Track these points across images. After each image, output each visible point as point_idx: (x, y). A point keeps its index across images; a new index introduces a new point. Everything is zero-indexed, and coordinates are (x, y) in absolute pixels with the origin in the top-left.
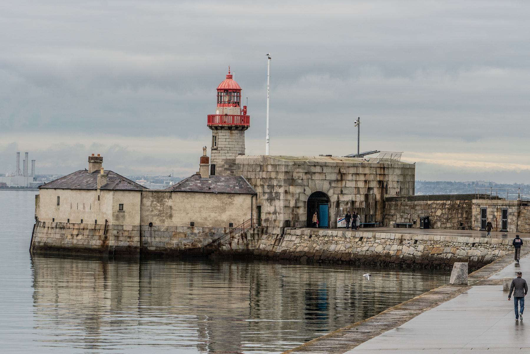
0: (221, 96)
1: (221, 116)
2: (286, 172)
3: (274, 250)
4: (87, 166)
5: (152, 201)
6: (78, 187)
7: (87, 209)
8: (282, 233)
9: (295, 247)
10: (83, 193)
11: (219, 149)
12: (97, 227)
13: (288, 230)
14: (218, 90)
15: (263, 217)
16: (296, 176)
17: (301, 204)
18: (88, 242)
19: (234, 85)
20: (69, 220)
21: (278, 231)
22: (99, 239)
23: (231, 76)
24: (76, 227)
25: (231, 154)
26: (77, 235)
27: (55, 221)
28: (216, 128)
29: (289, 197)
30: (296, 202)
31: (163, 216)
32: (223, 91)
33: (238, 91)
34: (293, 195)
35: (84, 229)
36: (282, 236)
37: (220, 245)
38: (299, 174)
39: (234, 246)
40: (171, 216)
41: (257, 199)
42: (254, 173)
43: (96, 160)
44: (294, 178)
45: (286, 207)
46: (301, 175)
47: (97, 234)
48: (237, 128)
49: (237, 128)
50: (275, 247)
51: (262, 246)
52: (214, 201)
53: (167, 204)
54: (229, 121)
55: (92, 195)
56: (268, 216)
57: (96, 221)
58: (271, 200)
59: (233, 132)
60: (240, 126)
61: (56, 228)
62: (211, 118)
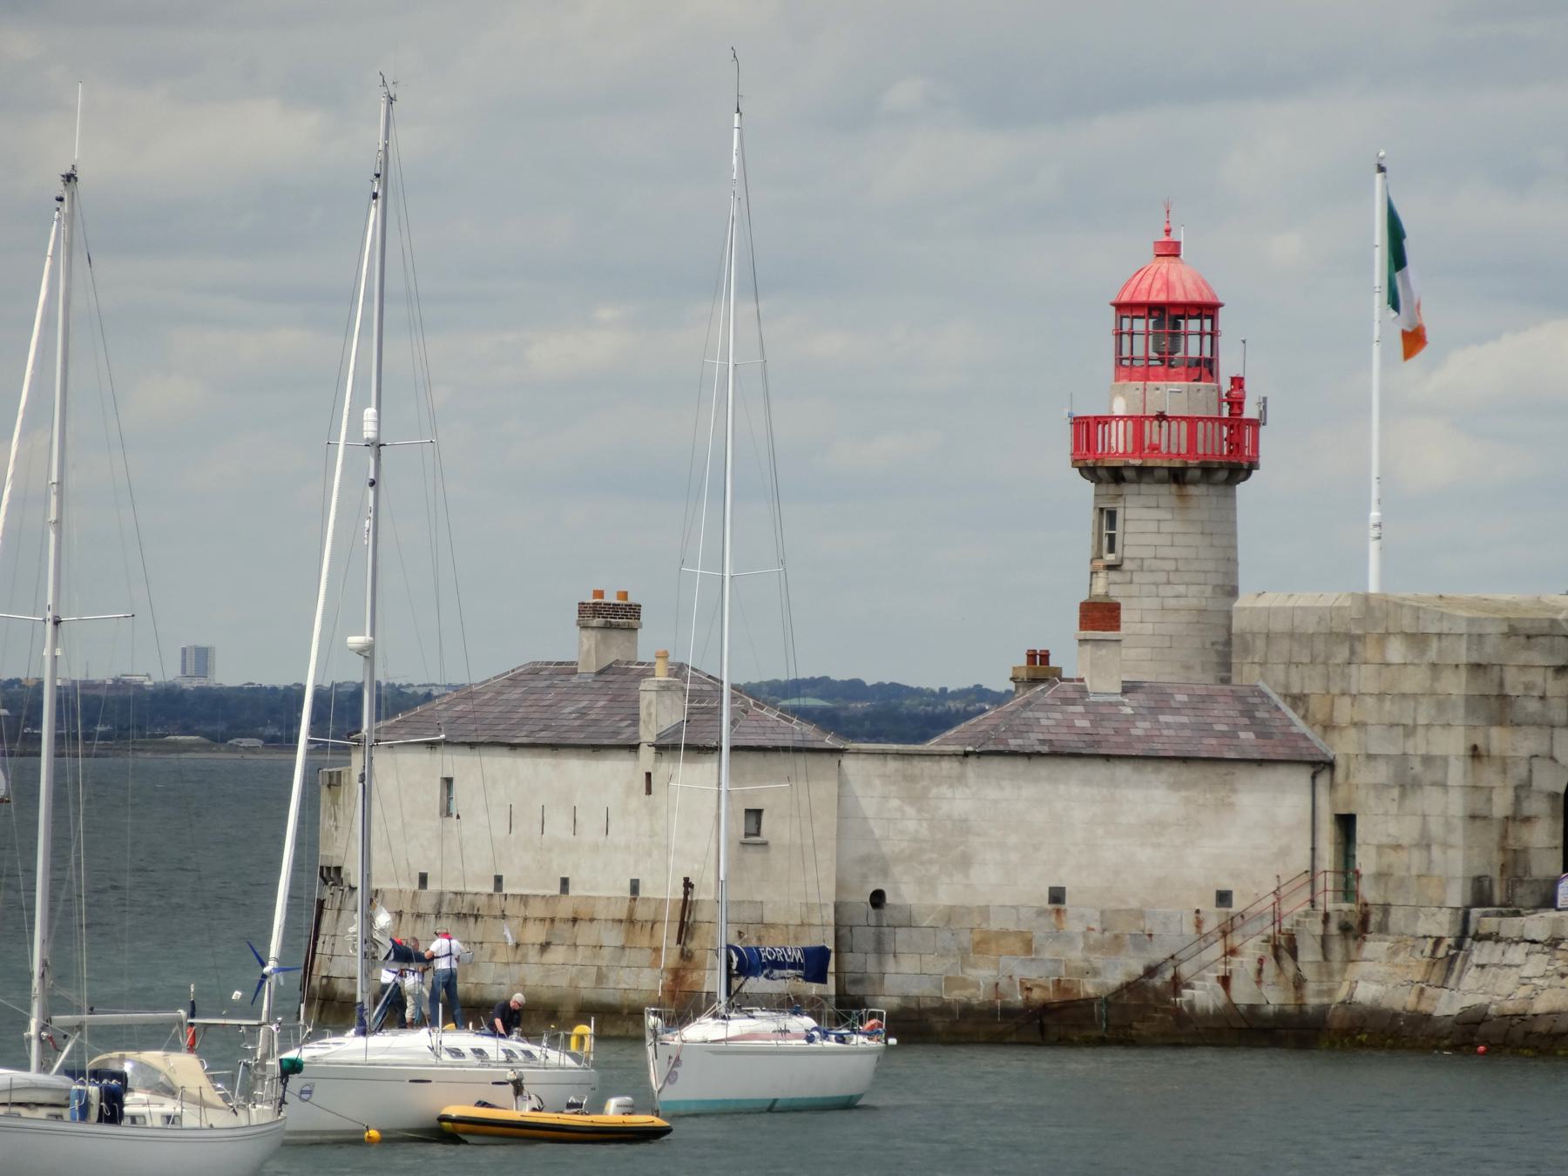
0: (1132, 334)
1: (1138, 421)
2: (1477, 668)
3: (1425, 1007)
4: (576, 646)
5: (885, 798)
6: (545, 737)
7: (591, 829)
8: (1457, 930)
9: (1523, 992)
10: (575, 768)
11: (1127, 565)
12: (642, 913)
13: (1484, 921)
14: (1120, 307)
15: (1365, 860)
16: (1514, 683)
17: (1537, 806)
18: (600, 978)
19: (1189, 285)
20: (498, 880)
21: (1441, 924)
22: (655, 964)
23: (1177, 244)
24: (537, 910)
25: (1181, 589)
26: (545, 947)
27: (433, 886)
28: (1116, 476)
29: (1489, 776)
30: (1518, 800)
31: (931, 862)
32: (1144, 312)
33: (1207, 310)
34: (1504, 765)
35: (575, 920)
36: (1459, 945)
37: (1177, 984)
38: (1527, 675)
39: (1243, 994)
40: (965, 862)
41: (1332, 785)
42: (1320, 669)
43: (613, 617)
44: (1509, 690)
45: (1473, 817)
46: (1539, 680)
47: (644, 941)
48: (1207, 471)
49: (1207, 471)
50: (1429, 991)
51: (1367, 993)
52: (1150, 797)
53: (945, 807)
54: (1171, 443)
55: (616, 772)
56: (1391, 857)
57: (635, 887)
58: (1406, 784)
59: (1192, 490)
60: (1221, 460)
61: (438, 915)
62: (1086, 429)
